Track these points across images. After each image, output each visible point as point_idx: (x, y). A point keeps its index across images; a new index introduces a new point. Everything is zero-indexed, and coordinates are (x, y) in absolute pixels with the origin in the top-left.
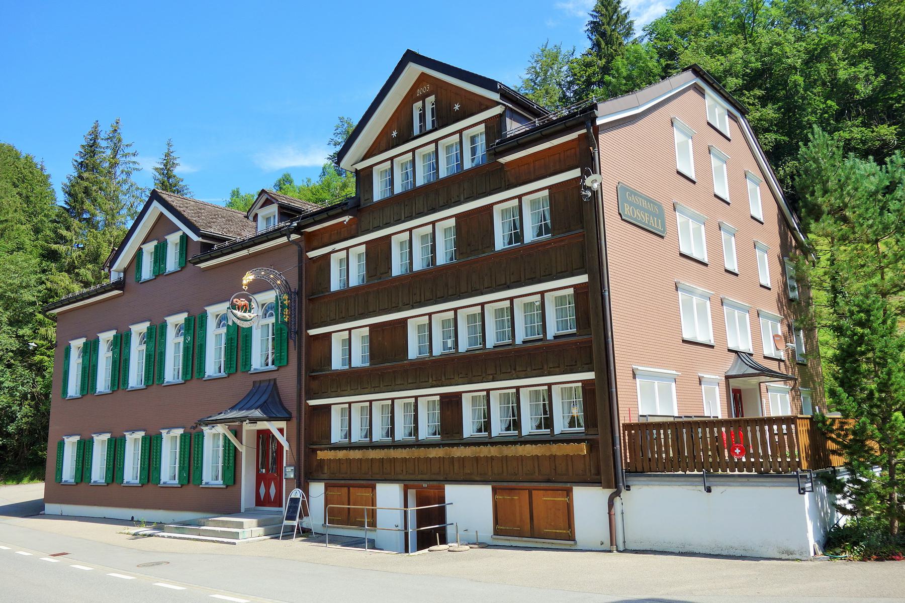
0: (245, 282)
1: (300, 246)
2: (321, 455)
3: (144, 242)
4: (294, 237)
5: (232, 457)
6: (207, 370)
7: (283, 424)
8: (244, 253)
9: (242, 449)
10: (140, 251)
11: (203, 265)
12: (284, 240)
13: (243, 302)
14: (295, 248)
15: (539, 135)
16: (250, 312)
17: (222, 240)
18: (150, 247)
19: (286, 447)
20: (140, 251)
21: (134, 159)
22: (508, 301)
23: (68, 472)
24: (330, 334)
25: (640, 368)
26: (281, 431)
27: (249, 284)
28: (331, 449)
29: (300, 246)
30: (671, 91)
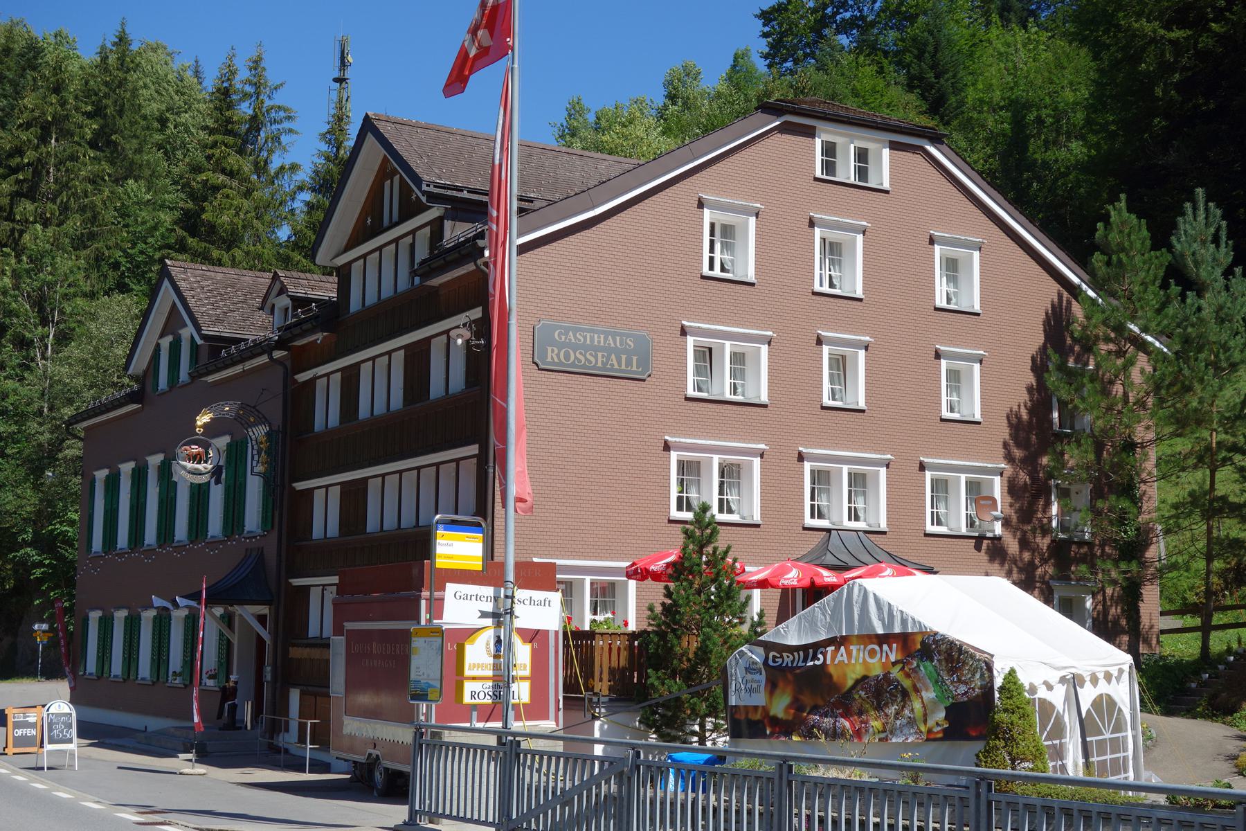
0: (199, 423)
1: (286, 367)
2: (295, 653)
3: (162, 336)
4: (277, 354)
5: (226, 648)
6: (147, 537)
7: (264, 610)
8: (238, 369)
9: (235, 642)
10: (158, 345)
11: (211, 378)
12: (264, 359)
13: (195, 449)
14: (280, 370)
15: (457, 255)
16: (206, 462)
17: (237, 341)
18: (166, 342)
19: (268, 642)
20: (158, 345)
21: (286, 125)
22: (434, 468)
23: (91, 665)
24: (313, 489)
25: (559, 562)
26: (262, 619)
27: (205, 426)
28: (307, 646)
29: (286, 367)
30: (692, 161)
